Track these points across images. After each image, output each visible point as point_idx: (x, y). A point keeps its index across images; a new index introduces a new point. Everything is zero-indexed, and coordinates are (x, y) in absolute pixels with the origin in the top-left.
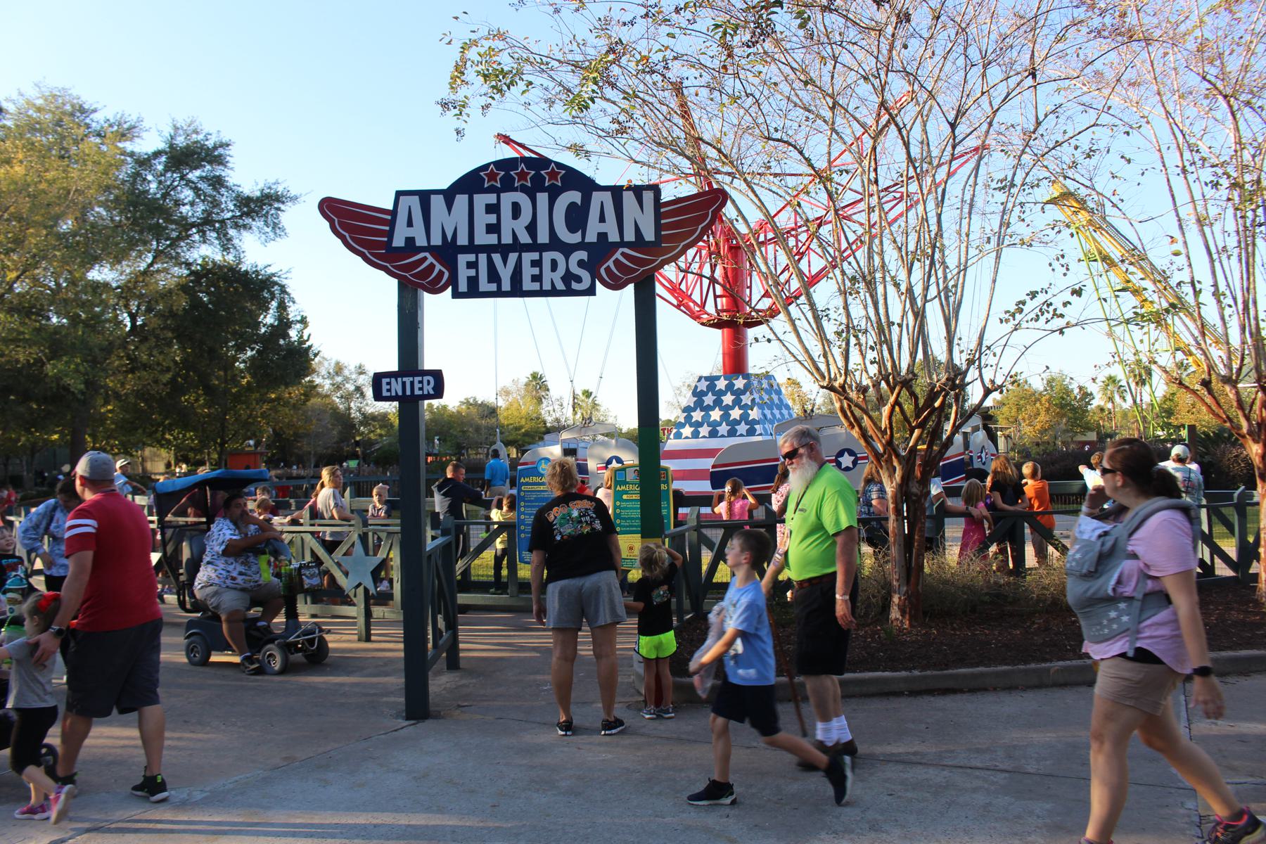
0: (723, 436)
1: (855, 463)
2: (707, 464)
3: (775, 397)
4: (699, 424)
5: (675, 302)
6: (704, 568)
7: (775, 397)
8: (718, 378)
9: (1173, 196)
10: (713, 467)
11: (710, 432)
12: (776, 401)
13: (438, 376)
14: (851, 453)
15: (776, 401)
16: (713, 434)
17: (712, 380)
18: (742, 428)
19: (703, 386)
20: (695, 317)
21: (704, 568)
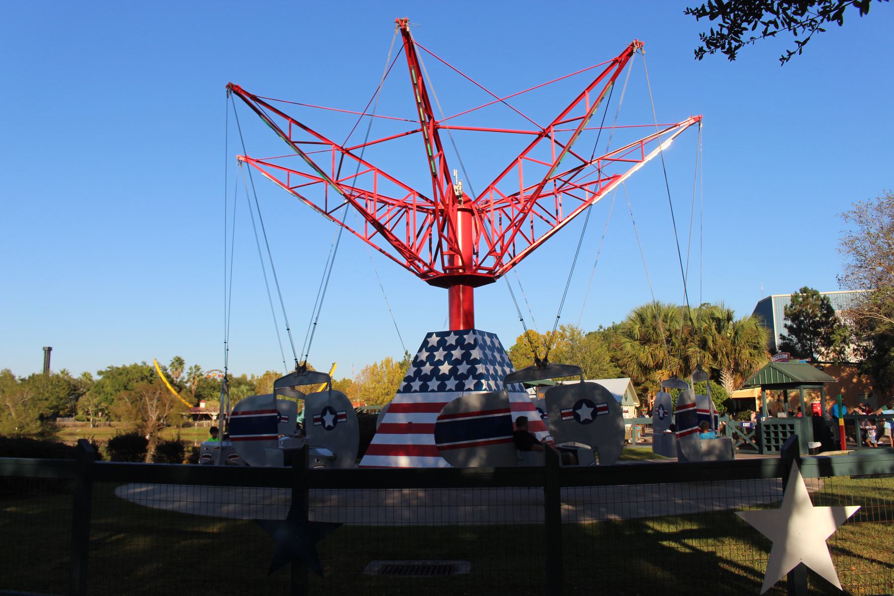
0: (433, 391)
1: (594, 414)
2: (431, 418)
3: (497, 355)
4: (465, 377)
5: (404, 262)
6: (688, 551)
7: (497, 355)
8: (447, 334)
9: (381, 250)
10: (439, 418)
11: (421, 387)
12: (499, 359)
13: (804, 290)
14: (590, 404)
15: (499, 359)
16: (442, 388)
17: (442, 335)
18: (451, 384)
19: (434, 340)
20: (423, 275)
21: (688, 551)
